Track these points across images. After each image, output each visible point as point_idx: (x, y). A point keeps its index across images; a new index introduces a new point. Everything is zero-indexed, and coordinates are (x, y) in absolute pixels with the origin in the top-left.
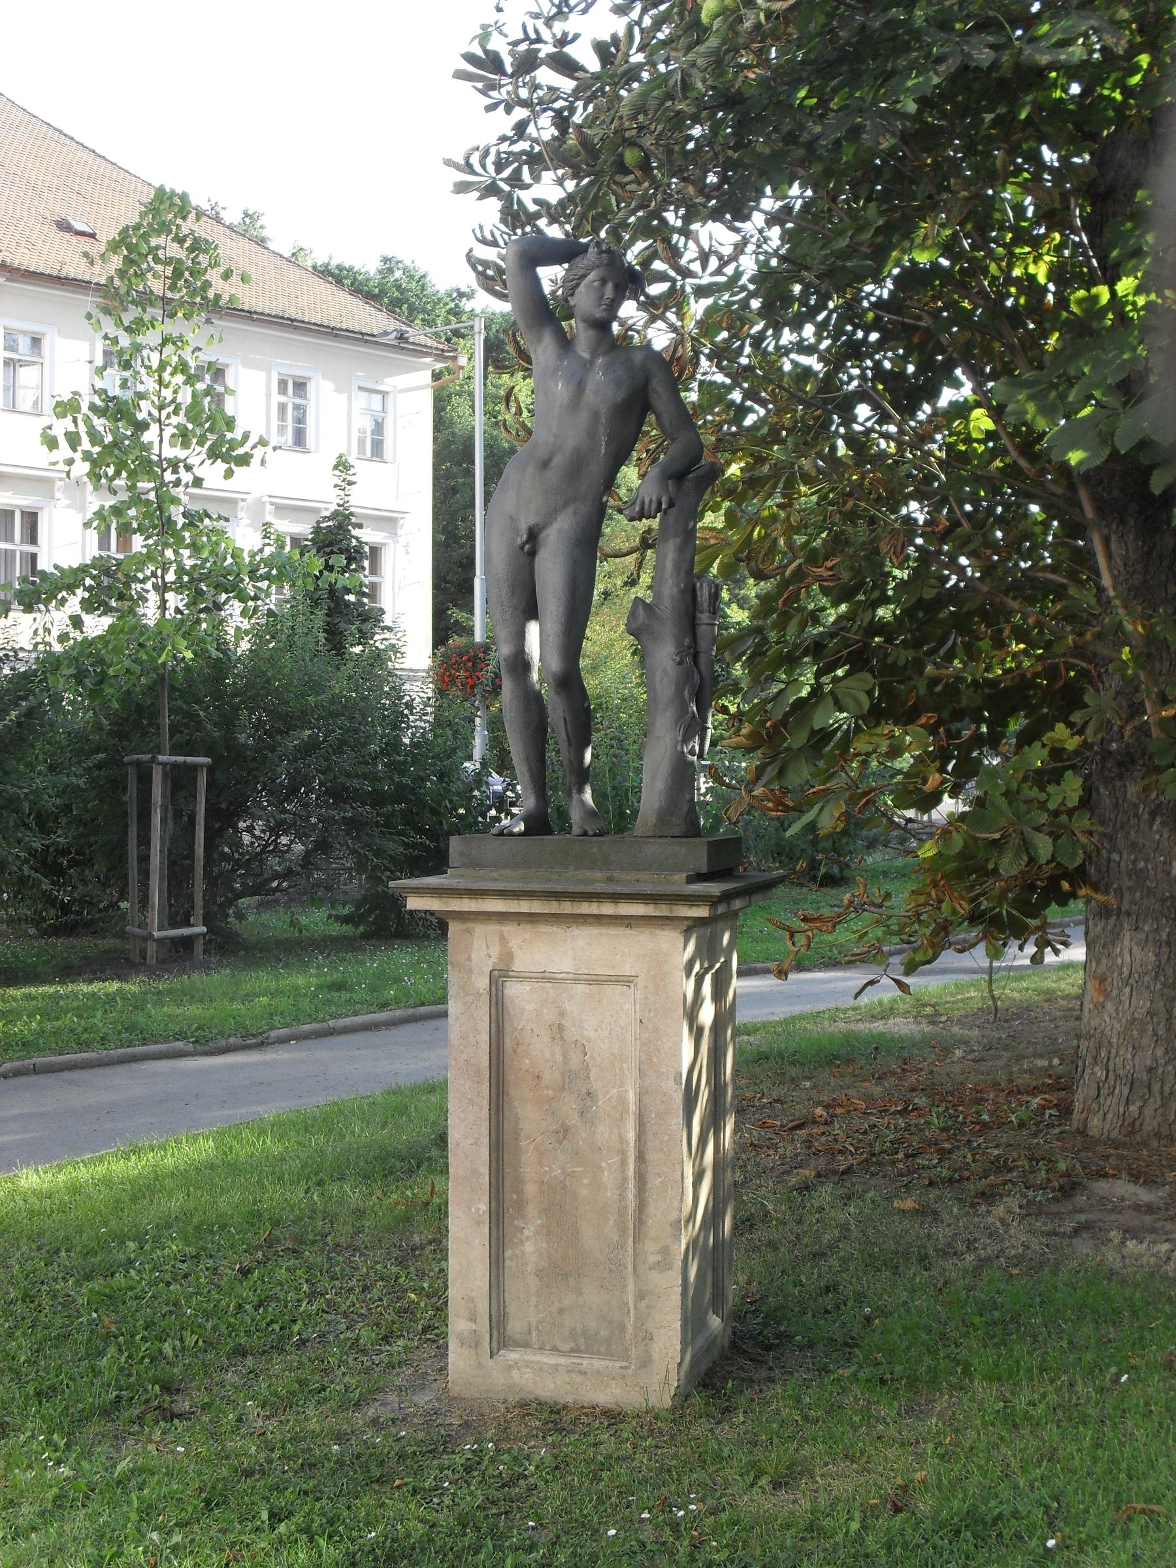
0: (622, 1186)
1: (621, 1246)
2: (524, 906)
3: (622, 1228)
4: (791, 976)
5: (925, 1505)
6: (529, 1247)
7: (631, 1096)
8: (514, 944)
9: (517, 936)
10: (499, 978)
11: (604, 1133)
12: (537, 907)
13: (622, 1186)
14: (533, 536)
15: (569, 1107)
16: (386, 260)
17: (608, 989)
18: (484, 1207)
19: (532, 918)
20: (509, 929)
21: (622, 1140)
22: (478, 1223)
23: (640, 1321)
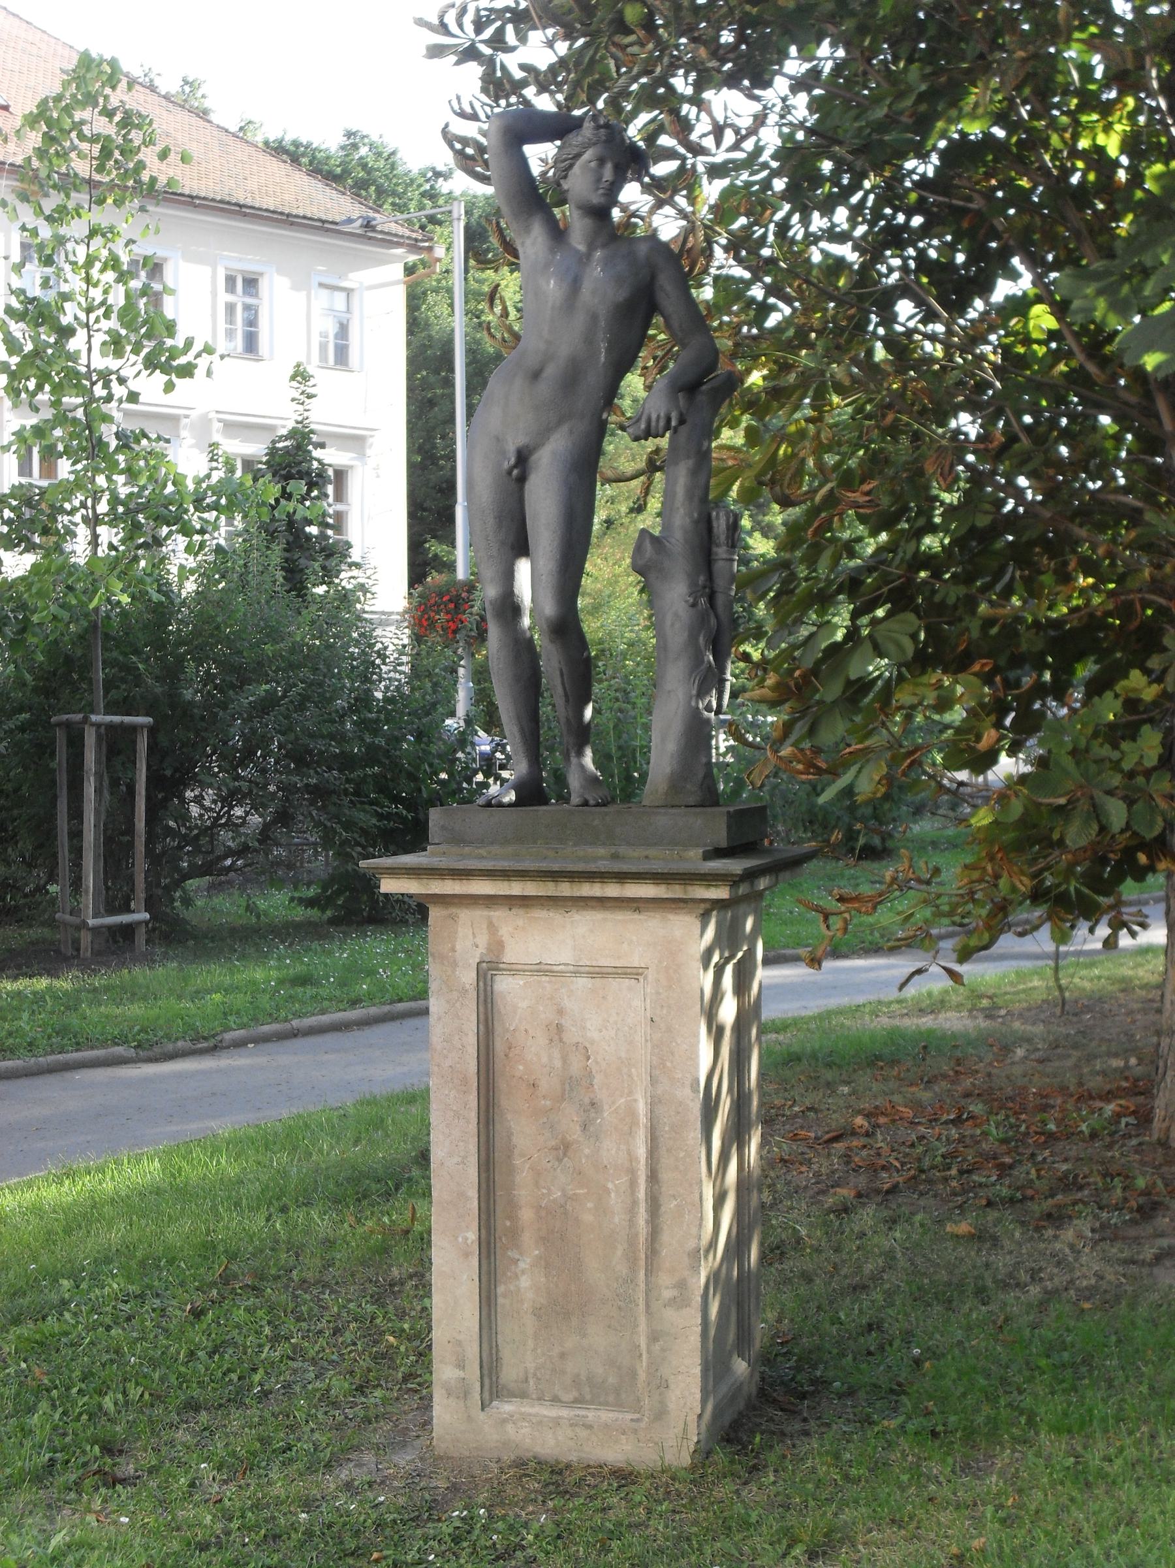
1: (631, 1280)
3: (632, 1261)
6: (525, 1282)
9: (508, 922)
11: (610, 1150)
17: (614, 984)
19: (524, 901)
20: (498, 914)
21: (632, 1158)
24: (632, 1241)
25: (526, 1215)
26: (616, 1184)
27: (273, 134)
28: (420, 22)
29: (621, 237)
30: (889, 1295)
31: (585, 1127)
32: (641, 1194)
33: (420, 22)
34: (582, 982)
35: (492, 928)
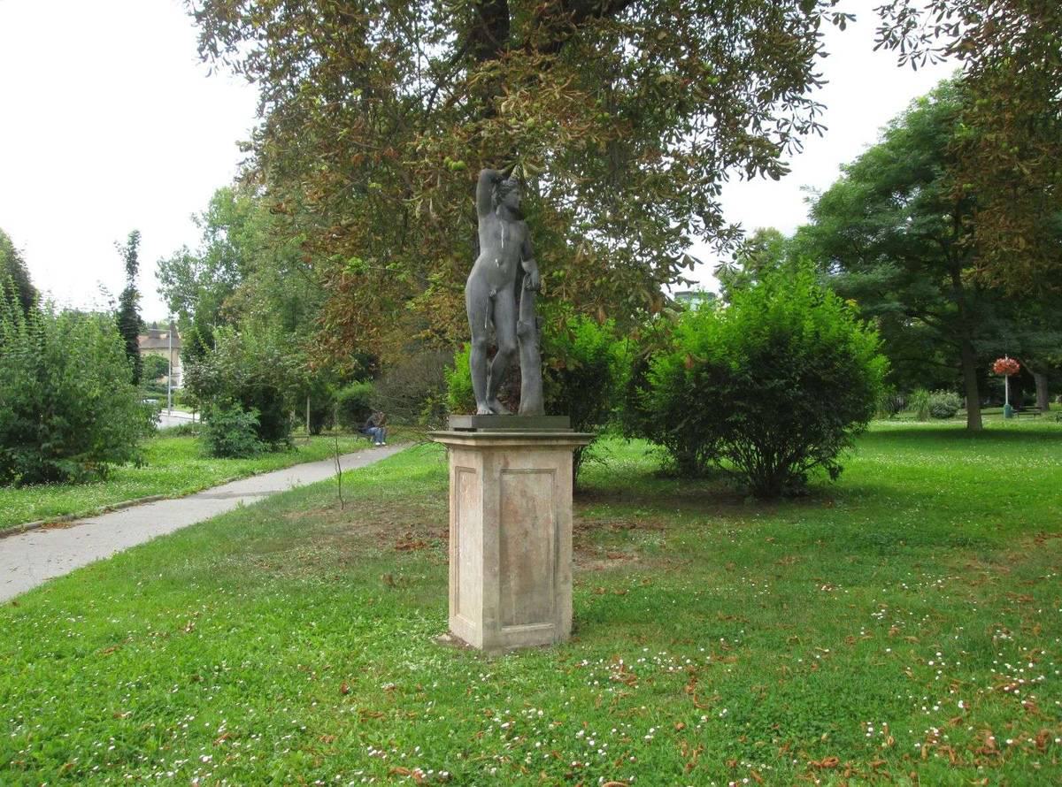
0: (548, 554)
1: (547, 577)
2: (523, 443)
3: (548, 569)
4: (879, 457)
5: (982, 555)
6: (512, 583)
7: (552, 517)
8: (509, 460)
9: (511, 456)
10: (472, 471)
11: (541, 533)
12: (528, 443)
13: (548, 554)
14: (493, 300)
15: (528, 525)
16: (716, 274)
17: (543, 476)
18: (497, 569)
19: (518, 448)
20: (508, 453)
21: (548, 534)
22: (495, 576)
23: (555, 608)
24: (548, 563)
25: (513, 559)
26: (543, 544)
27: (125, 274)
28: (875, 49)
29: (246, 398)
30: (994, 201)
31: (533, 525)
32: (552, 546)
33: (875, 49)
34: (532, 476)
35: (505, 459)
